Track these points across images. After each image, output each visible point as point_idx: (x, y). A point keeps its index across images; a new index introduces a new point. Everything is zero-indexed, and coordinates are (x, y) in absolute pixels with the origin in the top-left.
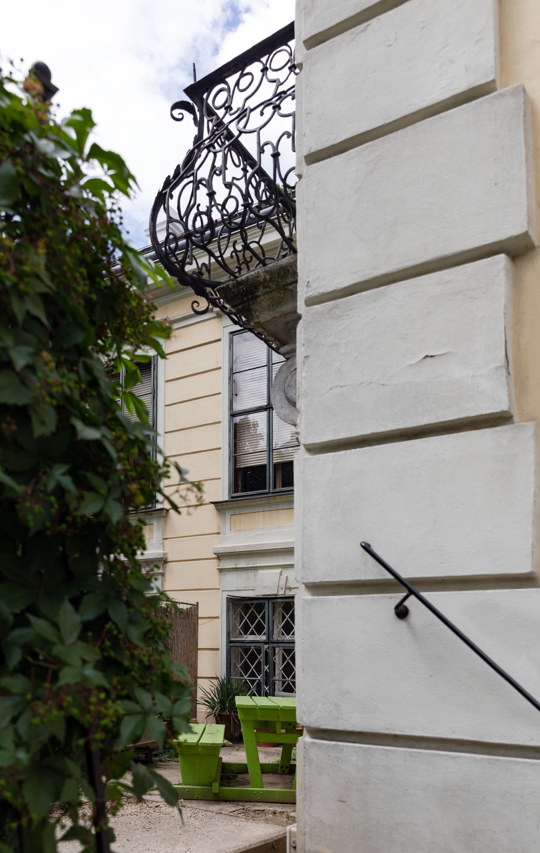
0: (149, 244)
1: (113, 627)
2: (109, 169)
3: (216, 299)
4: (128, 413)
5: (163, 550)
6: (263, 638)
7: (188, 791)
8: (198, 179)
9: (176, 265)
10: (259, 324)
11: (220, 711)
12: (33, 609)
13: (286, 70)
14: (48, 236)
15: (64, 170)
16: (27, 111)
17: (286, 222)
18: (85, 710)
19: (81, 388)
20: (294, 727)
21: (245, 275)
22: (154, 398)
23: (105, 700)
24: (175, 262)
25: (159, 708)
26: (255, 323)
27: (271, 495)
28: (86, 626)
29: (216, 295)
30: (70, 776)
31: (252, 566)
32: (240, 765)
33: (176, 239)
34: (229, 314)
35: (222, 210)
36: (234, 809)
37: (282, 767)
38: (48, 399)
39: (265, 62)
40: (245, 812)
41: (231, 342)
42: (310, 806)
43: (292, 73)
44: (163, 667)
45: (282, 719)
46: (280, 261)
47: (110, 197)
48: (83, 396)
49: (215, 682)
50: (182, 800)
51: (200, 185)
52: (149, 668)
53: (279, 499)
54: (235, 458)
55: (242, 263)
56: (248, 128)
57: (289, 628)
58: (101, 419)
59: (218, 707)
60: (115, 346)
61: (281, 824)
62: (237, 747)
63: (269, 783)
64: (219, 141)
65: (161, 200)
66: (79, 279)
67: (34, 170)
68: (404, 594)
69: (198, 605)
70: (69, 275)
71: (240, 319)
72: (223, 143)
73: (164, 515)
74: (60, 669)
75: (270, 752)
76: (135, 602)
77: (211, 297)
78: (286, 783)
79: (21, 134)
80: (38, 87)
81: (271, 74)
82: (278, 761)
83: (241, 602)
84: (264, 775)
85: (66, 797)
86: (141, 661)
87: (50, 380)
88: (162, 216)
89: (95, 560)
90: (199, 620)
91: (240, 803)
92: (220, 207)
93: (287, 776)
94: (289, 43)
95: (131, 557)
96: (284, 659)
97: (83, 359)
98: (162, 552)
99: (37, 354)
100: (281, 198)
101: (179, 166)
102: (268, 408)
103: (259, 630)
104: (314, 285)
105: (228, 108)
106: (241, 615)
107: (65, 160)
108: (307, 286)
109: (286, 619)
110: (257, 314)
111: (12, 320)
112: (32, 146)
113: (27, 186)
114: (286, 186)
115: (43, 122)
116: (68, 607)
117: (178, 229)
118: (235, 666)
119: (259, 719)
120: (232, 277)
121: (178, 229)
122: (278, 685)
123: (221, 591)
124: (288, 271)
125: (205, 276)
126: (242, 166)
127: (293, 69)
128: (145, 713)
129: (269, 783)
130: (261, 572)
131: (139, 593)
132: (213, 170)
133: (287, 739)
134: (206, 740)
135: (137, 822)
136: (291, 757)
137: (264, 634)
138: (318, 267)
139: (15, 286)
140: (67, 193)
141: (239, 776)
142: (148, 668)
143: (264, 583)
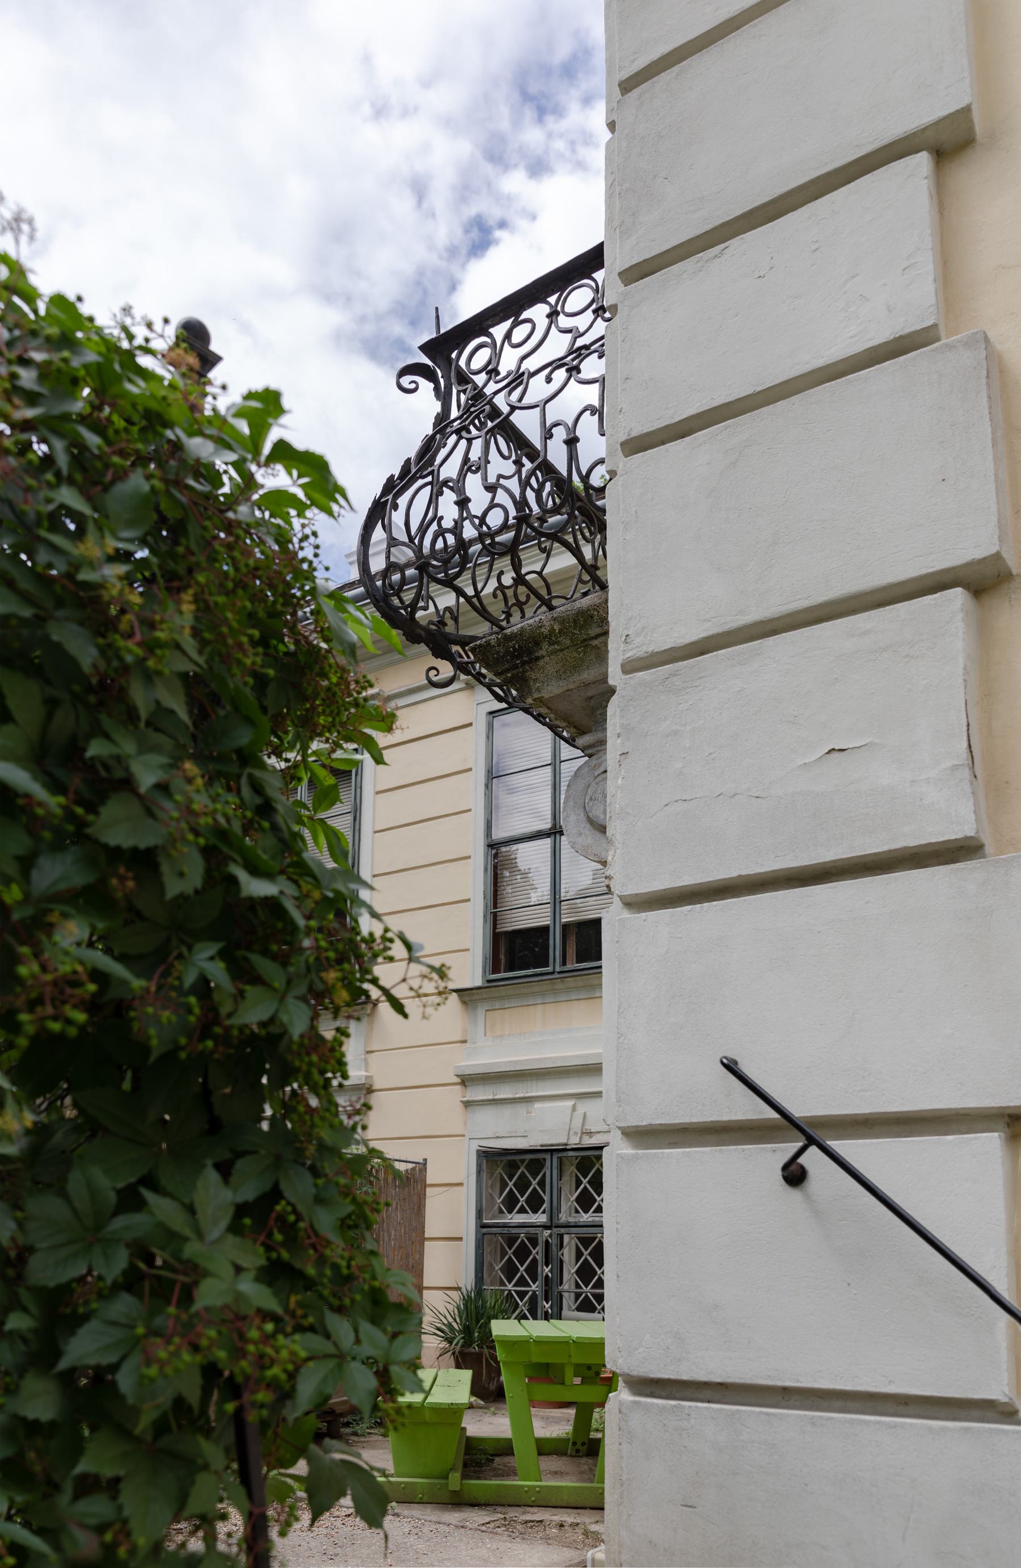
0: (354, 574)
1: (289, 1209)
2: (300, 476)
3: (467, 663)
4: (318, 853)
5: (366, 1071)
6: (541, 1218)
7: (404, 1488)
8: (441, 479)
9: (403, 611)
10: (540, 701)
11: (463, 1346)
12: (150, 1182)
13: (589, 315)
14: (197, 583)
15: (225, 478)
16: (172, 396)
17: (587, 541)
18: (239, 1353)
19: (244, 817)
20: (598, 1373)
21: (516, 624)
22: (355, 820)
23: (273, 1336)
24: (400, 608)
25: (366, 1350)
26: (535, 700)
27: (557, 976)
28: (241, 1210)
29: (468, 657)
30: (206, 1467)
31: (522, 1095)
32: (498, 1440)
33: (402, 568)
34: (489, 687)
35: (481, 525)
36: (488, 1519)
37: (574, 1444)
38: (190, 837)
39: (553, 303)
40: (508, 1524)
41: (490, 727)
42: (629, 1515)
43: (599, 319)
44: (374, 1278)
45: (575, 1360)
46: (577, 603)
47: (299, 515)
48: (248, 827)
49: (455, 1295)
50: (394, 1504)
51: (444, 489)
52: (349, 1279)
53: (570, 982)
54: (495, 915)
55: (513, 605)
56: (526, 401)
57: (587, 1202)
58: (276, 866)
59: (459, 1339)
60: (298, 746)
61: (572, 1545)
62: (492, 1409)
63: (551, 1473)
64: (476, 421)
65: (378, 511)
66: (247, 646)
67: (179, 484)
68: (800, 1144)
69: (425, 1164)
70: (230, 641)
71: (507, 693)
72: (483, 424)
73: (369, 1011)
74: (196, 1283)
75: (553, 1418)
76: (328, 1168)
77: (459, 660)
78: (581, 1473)
79: (159, 429)
80: (192, 360)
81: (563, 321)
82: (567, 1434)
83: (503, 1158)
84: (542, 1458)
85: (194, 1505)
86: (335, 1267)
87: (195, 807)
88: (379, 534)
89: (259, 1096)
90: (428, 1189)
91: (499, 1509)
92: (477, 521)
93: (584, 1460)
94: (594, 275)
95: (322, 1092)
96: (579, 1254)
97: (249, 770)
98: (364, 1073)
99: (175, 765)
100: (579, 504)
101: (409, 460)
102: (555, 832)
103: (535, 1204)
104: (638, 641)
105: (492, 372)
106: (502, 1180)
107: (226, 464)
108: (626, 642)
109: (582, 1186)
110: (538, 684)
111: (131, 716)
112: (177, 447)
113: (163, 506)
114: (587, 486)
115: (195, 408)
116: (212, 1176)
117: (404, 555)
118: (491, 1267)
119: (535, 1359)
120: (495, 629)
121: (404, 555)
122: (568, 1300)
123: (466, 1139)
124: (592, 617)
125: (450, 628)
126: (514, 458)
127: (600, 312)
128: (341, 1357)
129: (551, 1473)
130: (537, 1105)
131: (334, 1151)
132: (467, 466)
133: (588, 1394)
134: (439, 1397)
135: (312, 1544)
136: (590, 1426)
137: (544, 1212)
138: (640, 612)
139: (141, 661)
140: (231, 515)
141: (497, 1459)
142: (345, 1280)
143: (544, 1124)
